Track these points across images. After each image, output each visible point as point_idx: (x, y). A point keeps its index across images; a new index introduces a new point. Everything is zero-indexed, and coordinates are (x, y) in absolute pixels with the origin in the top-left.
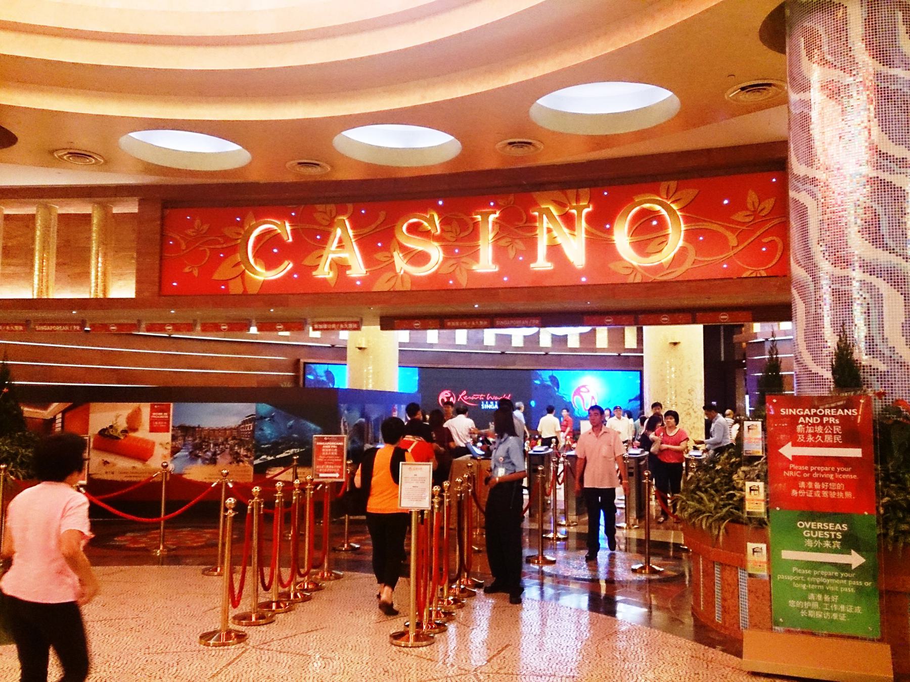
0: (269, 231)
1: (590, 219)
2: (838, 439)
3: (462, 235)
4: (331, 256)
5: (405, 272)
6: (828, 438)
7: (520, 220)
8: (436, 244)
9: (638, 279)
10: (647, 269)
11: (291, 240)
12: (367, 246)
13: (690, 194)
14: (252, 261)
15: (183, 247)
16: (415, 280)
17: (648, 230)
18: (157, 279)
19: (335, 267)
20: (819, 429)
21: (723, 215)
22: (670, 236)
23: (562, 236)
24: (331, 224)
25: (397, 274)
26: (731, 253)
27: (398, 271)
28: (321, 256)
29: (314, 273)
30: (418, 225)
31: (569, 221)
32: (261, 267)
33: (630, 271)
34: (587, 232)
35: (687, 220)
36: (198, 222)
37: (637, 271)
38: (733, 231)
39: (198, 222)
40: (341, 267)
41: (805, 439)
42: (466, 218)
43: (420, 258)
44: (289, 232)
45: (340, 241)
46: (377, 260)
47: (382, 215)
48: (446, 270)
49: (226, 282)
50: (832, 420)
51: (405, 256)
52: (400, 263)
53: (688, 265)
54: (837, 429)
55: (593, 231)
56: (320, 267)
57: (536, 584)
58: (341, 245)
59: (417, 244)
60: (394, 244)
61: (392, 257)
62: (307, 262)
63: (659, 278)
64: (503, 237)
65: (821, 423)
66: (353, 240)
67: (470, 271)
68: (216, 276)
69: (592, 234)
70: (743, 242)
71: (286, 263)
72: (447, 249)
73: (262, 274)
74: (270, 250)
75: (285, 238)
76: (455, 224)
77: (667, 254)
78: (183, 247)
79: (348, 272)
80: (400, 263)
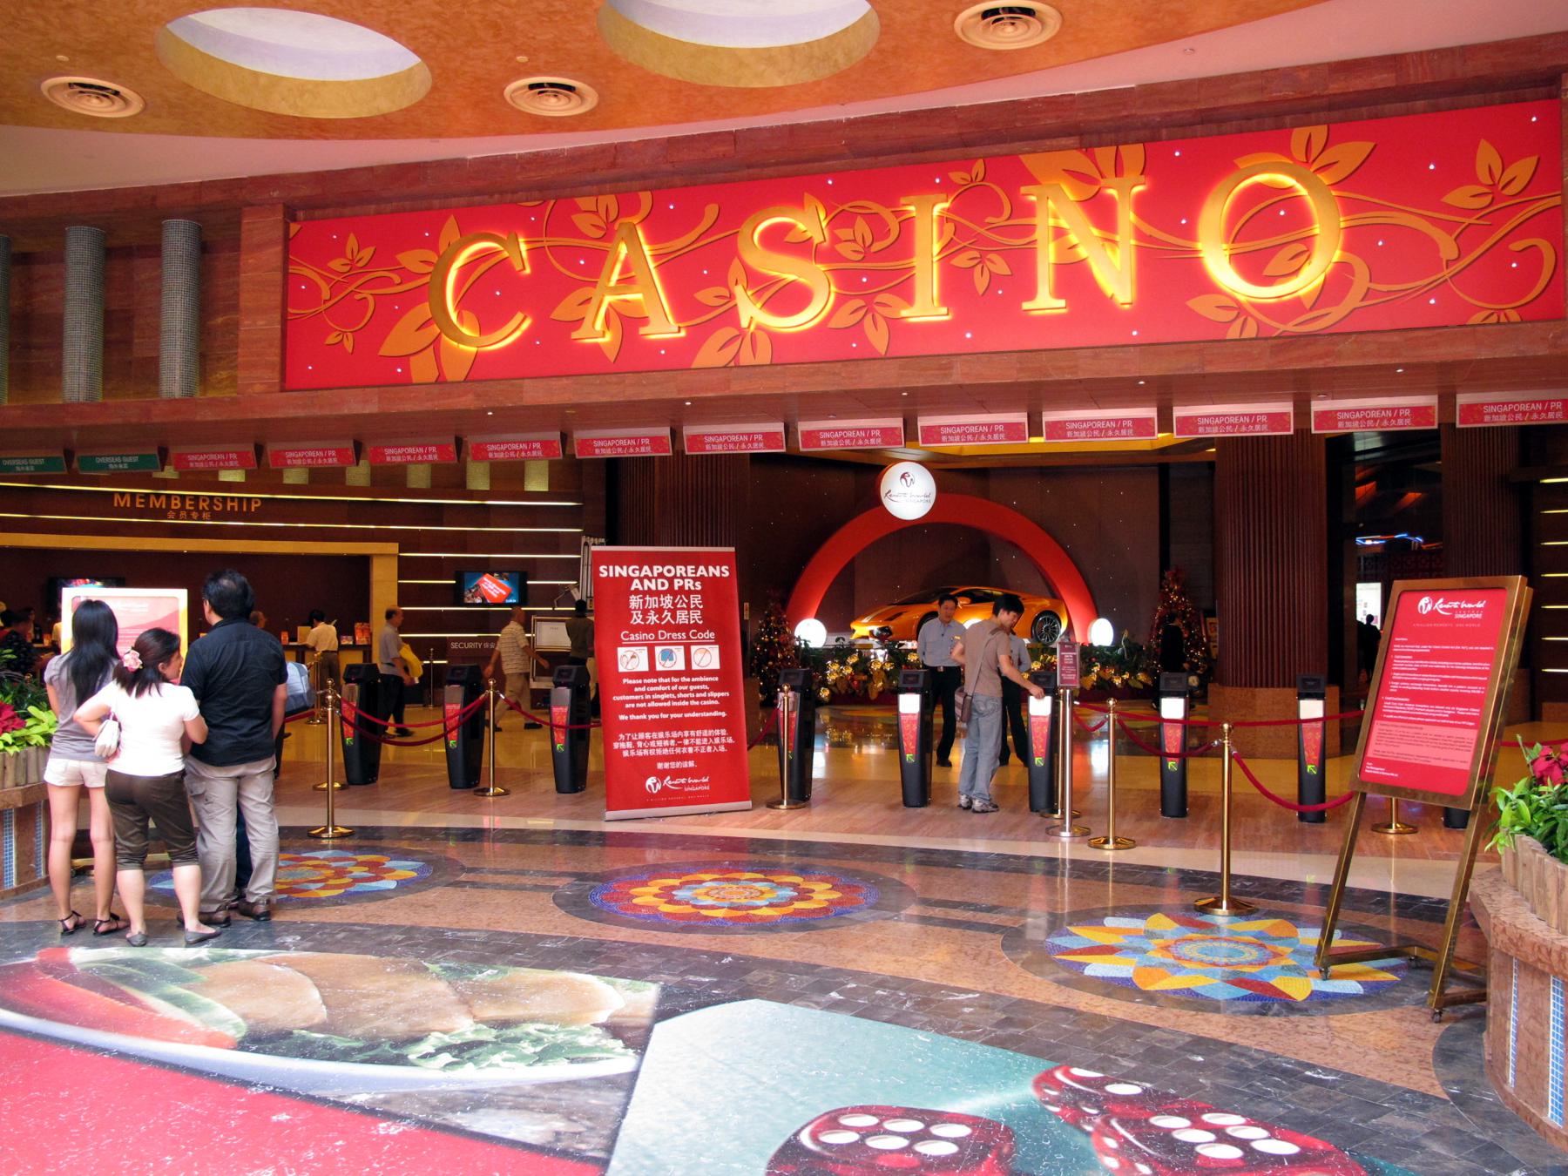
0: (485, 255)
1: (1143, 206)
2: (696, 616)
3: (877, 247)
4: (608, 299)
5: (759, 327)
6: (682, 617)
7: (999, 213)
8: (822, 267)
9: (1251, 331)
10: (1263, 308)
11: (528, 271)
12: (684, 281)
13: (1353, 153)
14: (454, 316)
15: (326, 294)
16: (775, 338)
17: (1268, 232)
18: (277, 359)
19: (616, 322)
20: (667, 601)
21: (1427, 195)
22: (1318, 242)
23: (1085, 242)
24: (609, 235)
25: (742, 332)
26: (1447, 273)
27: (744, 324)
28: (588, 301)
29: (574, 335)
30: (786, 228)
31: (1101, 212)
32: (471, 328)
33: (1235, 313)
34: (1139, 235)
35: (1349, 207)
36: (352, 242)
37: (1248, 314)
38: (1447, 227)
39: (352, 242)
40: (629, 322)
41: (644, 619)
42: (886, 213)
43: (790, 298)
44: (524, 255)
45: (626, 268)
46: (700, 304)
47: (711, 212)
48: (844, 319)
49: (403, 360)
50: (689, 584)
51: (758, 295)
52: (751, 312)
53: (1353, 300)
54: (696, 600)
55: (1149, 230)
56: (587, 324)
57: (860, 747)
58: (627, 280)
59: (788, 270)
60: (735, 270)
61: (732, 297)
62: (562, 313)
63: (1291, 327)
64: (964, 249)
65: (671, 591)
66: (652, 265)
67: (895, 325)
68: (386, 350)
69: (1150, 239)
70: (1469, 252)
71: (520, 316)
72: (847, 281)
73: (469, 341)
74: (489, 295)
75: (518, 267)
76: (862, 227)
77: (1308, 280)
78: (326, 294)
79: (642, 331)
80: (751, 312)
